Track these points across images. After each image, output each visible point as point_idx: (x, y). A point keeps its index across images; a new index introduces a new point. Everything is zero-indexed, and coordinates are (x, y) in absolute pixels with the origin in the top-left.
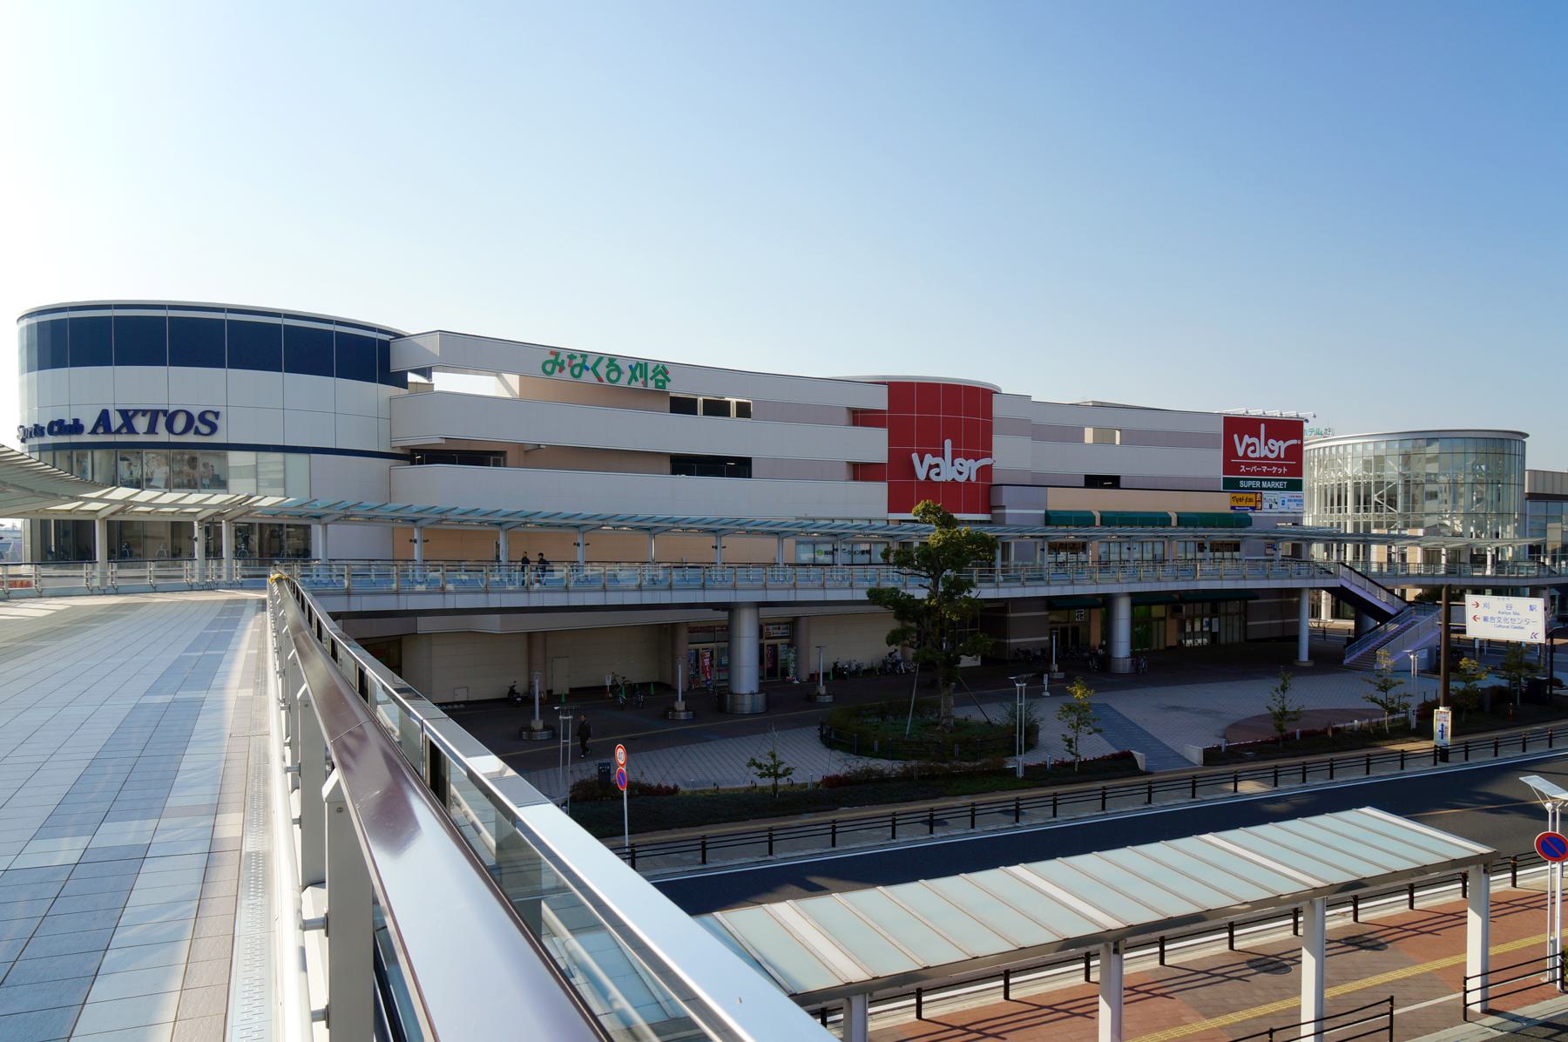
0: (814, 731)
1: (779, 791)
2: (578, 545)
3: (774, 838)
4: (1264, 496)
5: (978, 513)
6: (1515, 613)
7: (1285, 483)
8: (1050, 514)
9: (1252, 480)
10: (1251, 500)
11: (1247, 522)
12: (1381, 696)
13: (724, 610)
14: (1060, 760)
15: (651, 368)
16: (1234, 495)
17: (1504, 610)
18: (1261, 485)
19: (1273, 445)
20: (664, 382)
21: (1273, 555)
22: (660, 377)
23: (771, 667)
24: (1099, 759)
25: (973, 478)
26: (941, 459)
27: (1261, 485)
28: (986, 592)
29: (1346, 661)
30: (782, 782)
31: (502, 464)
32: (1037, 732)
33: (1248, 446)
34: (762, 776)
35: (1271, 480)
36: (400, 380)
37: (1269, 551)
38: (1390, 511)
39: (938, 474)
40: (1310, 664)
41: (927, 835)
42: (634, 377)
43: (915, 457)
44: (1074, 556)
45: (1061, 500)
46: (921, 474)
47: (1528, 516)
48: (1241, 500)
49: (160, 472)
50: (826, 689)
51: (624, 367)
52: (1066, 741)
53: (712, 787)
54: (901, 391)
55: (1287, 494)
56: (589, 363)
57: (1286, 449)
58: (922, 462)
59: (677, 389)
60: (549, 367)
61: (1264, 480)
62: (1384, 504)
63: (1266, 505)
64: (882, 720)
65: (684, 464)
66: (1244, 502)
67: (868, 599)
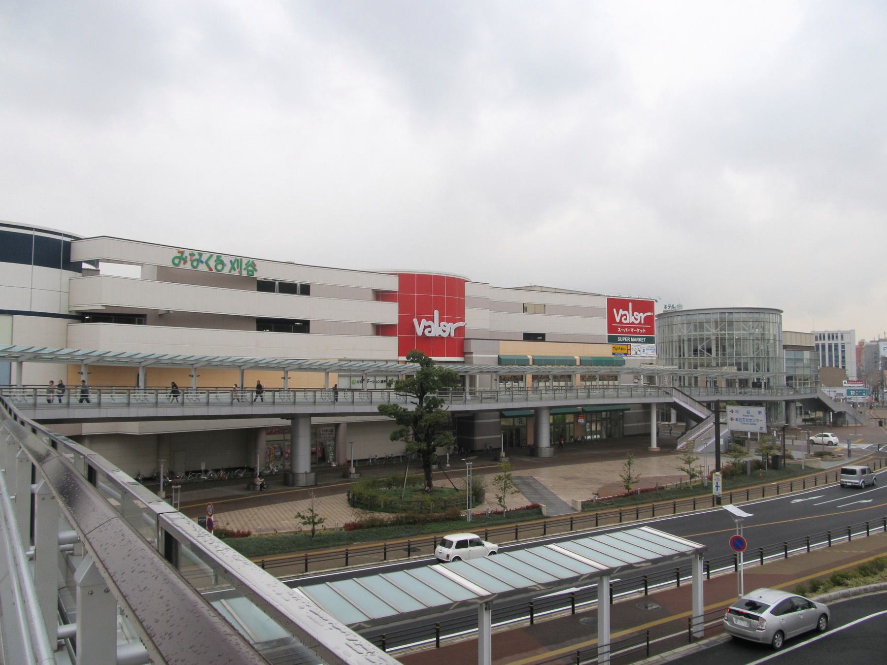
0: (344, 496)
1: (316, 534)
2: (192, 376)
3: (308, 561)
4: (632, 347)
5: (455, 356)
6: (751, 416)
7: (645, 339)
8: (502, 357)
9: (625, 336)
10: (624, 349)
11: (623, 363)
12: (687, 467)
13: (288, 419)
14: (495, 510)
15: (245, 261)
16: (614, 346)
17: (746, 414)
18: (630, 340)
19: (637, 315)
20: (253, 272)
21: (637, 383)
22: (250, 268)
23: (320, 457)
24: (519, 510)
25: (452, 335)
26: (432, 322)
27: (630, 340)
28: (457, 406)
29: (679, 447)
30: (318, 527)
31: (144, 323)
32: (484, 494)
33: (622, 316)
34: (305, 523)
35: (636, 337)
36: (76, 267)
37: (636, 381)
38: (709, 356)
39: (430, 332)
40: (658, 449)
41: (406, 557)
42: (233, 268)
43: (415, 321)
44: (516, 384)
45: (510, 349)
46: (419, 331)
47: (785, 359)
48: (618, 349)
49: (393, 416)
50: (356, 470)
51: (226, 260)
52: (497, 498)
53: (273, 532)
54: (405, 279)
55: (646, 346)
56: (204, 258)
57: (645, 318)
58: (419, 324)
59: (262, 274)
60: (177, 261)
61: (633, 337)
62: (705, 351)
63: (633, 352)
64: (389, 488)
65: (265, 324)
66: (620, 350)
67: (378, 411)
